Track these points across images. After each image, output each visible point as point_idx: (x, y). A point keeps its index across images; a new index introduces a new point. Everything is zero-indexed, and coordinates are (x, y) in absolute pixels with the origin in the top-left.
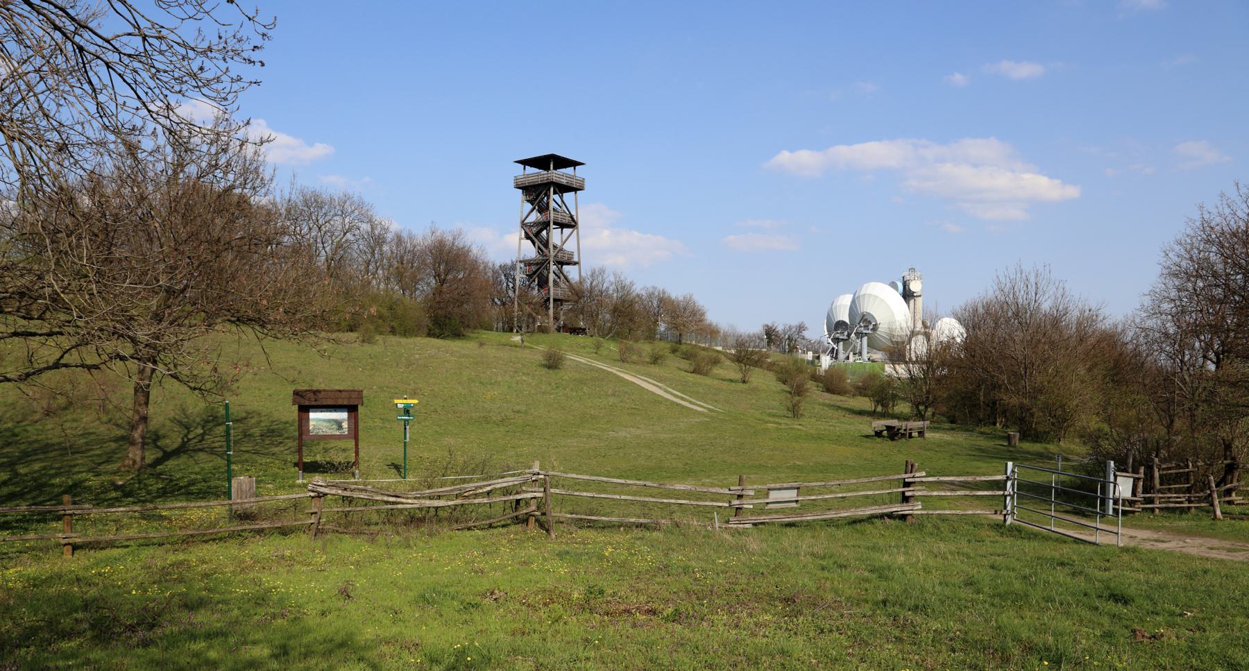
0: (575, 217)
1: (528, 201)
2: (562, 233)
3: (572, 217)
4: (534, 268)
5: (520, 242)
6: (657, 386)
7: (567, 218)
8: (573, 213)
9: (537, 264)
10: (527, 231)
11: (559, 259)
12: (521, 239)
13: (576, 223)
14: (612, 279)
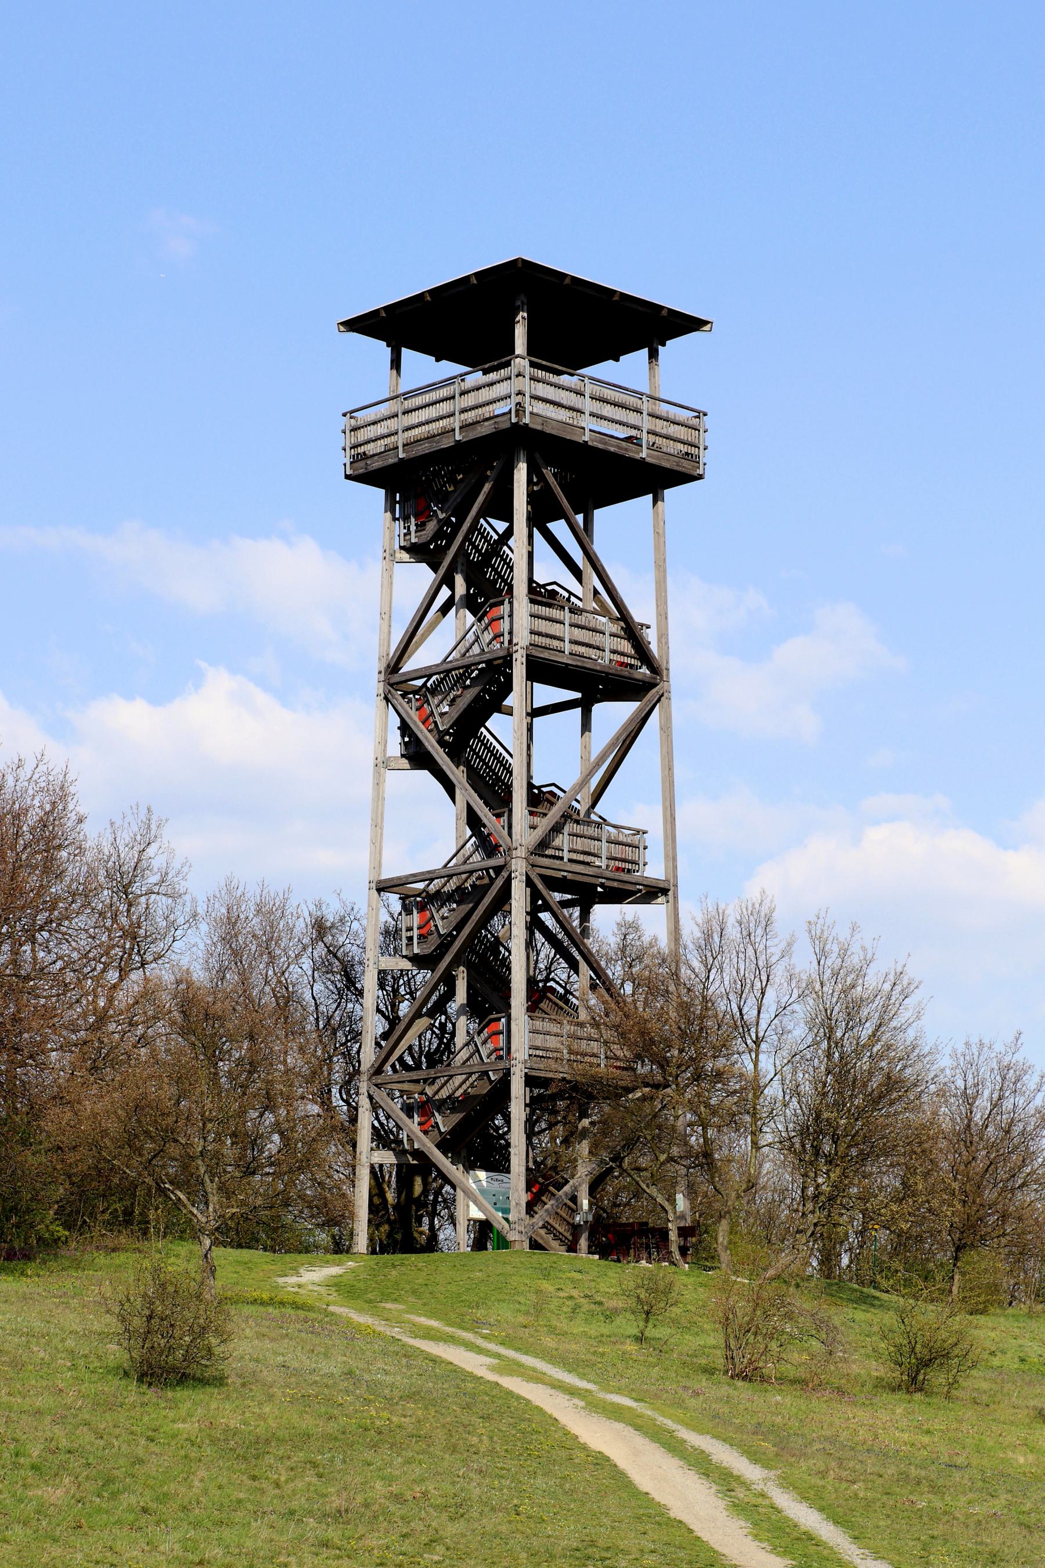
0: (651, 637)
1: (417, 552)
2: (586, 725)
3: (631, 631)
4: (443, 918)
5: (378, 784)
6: (547, 636)
7: (608, 643)
8: (641, 612)
9: (460, 895)
10: (414, 718)
11: (565, 869)
12: (383, 764)
13: (655, 670)
14: (804, 962)
